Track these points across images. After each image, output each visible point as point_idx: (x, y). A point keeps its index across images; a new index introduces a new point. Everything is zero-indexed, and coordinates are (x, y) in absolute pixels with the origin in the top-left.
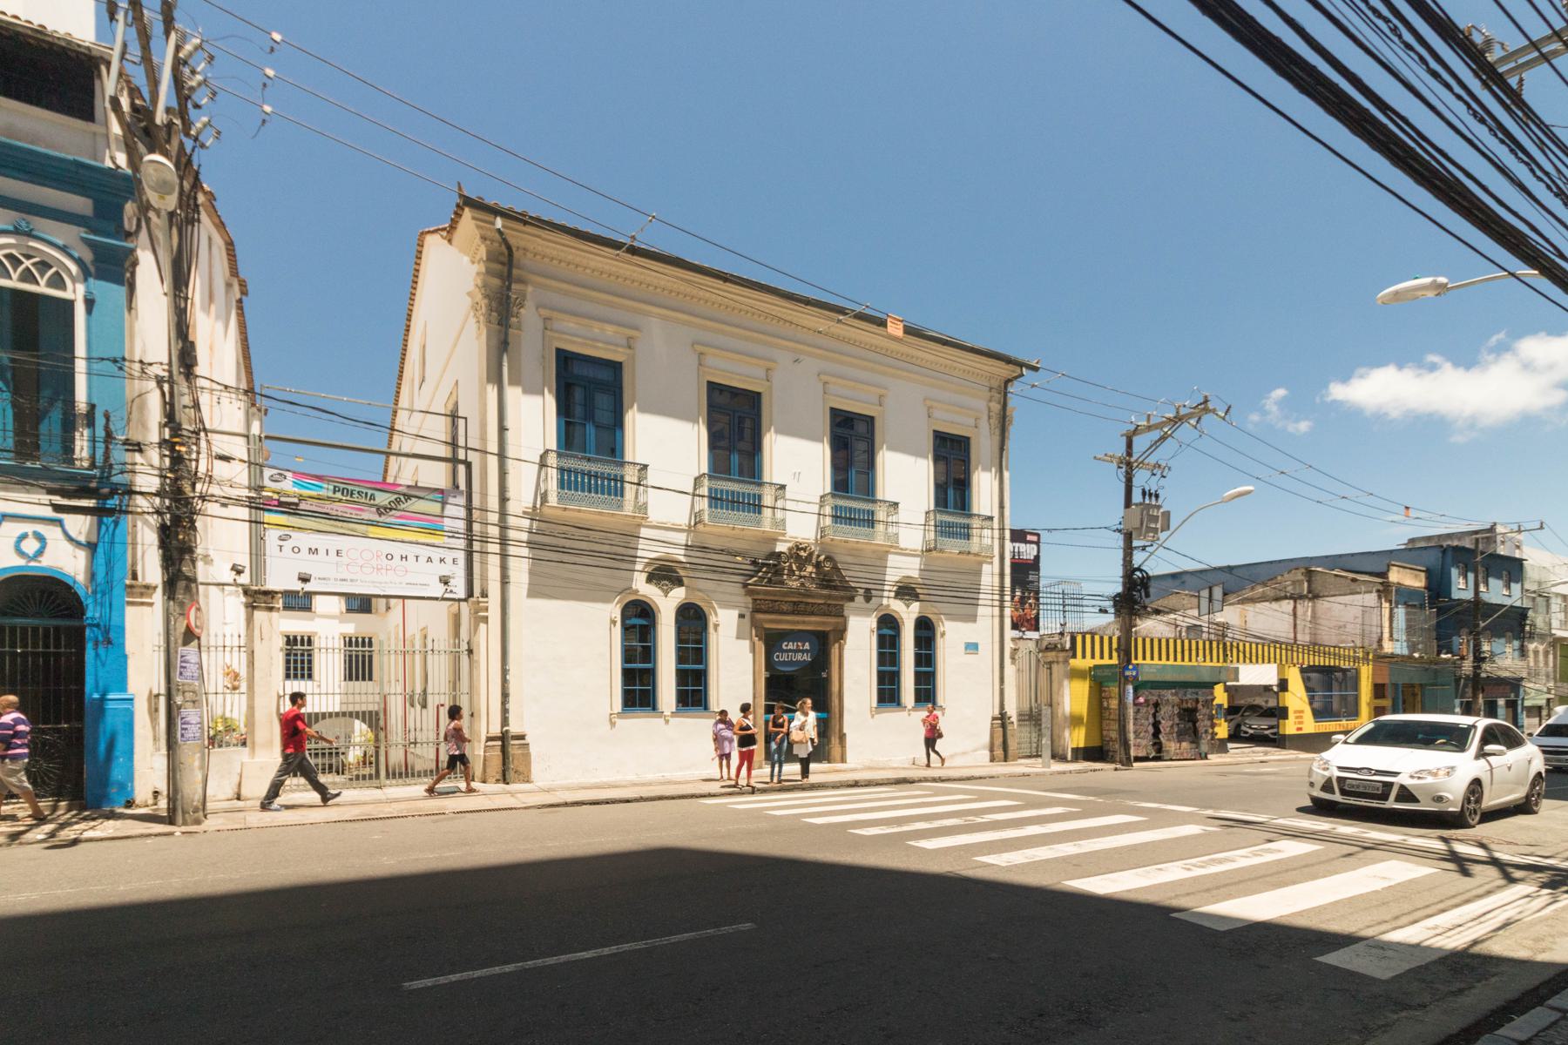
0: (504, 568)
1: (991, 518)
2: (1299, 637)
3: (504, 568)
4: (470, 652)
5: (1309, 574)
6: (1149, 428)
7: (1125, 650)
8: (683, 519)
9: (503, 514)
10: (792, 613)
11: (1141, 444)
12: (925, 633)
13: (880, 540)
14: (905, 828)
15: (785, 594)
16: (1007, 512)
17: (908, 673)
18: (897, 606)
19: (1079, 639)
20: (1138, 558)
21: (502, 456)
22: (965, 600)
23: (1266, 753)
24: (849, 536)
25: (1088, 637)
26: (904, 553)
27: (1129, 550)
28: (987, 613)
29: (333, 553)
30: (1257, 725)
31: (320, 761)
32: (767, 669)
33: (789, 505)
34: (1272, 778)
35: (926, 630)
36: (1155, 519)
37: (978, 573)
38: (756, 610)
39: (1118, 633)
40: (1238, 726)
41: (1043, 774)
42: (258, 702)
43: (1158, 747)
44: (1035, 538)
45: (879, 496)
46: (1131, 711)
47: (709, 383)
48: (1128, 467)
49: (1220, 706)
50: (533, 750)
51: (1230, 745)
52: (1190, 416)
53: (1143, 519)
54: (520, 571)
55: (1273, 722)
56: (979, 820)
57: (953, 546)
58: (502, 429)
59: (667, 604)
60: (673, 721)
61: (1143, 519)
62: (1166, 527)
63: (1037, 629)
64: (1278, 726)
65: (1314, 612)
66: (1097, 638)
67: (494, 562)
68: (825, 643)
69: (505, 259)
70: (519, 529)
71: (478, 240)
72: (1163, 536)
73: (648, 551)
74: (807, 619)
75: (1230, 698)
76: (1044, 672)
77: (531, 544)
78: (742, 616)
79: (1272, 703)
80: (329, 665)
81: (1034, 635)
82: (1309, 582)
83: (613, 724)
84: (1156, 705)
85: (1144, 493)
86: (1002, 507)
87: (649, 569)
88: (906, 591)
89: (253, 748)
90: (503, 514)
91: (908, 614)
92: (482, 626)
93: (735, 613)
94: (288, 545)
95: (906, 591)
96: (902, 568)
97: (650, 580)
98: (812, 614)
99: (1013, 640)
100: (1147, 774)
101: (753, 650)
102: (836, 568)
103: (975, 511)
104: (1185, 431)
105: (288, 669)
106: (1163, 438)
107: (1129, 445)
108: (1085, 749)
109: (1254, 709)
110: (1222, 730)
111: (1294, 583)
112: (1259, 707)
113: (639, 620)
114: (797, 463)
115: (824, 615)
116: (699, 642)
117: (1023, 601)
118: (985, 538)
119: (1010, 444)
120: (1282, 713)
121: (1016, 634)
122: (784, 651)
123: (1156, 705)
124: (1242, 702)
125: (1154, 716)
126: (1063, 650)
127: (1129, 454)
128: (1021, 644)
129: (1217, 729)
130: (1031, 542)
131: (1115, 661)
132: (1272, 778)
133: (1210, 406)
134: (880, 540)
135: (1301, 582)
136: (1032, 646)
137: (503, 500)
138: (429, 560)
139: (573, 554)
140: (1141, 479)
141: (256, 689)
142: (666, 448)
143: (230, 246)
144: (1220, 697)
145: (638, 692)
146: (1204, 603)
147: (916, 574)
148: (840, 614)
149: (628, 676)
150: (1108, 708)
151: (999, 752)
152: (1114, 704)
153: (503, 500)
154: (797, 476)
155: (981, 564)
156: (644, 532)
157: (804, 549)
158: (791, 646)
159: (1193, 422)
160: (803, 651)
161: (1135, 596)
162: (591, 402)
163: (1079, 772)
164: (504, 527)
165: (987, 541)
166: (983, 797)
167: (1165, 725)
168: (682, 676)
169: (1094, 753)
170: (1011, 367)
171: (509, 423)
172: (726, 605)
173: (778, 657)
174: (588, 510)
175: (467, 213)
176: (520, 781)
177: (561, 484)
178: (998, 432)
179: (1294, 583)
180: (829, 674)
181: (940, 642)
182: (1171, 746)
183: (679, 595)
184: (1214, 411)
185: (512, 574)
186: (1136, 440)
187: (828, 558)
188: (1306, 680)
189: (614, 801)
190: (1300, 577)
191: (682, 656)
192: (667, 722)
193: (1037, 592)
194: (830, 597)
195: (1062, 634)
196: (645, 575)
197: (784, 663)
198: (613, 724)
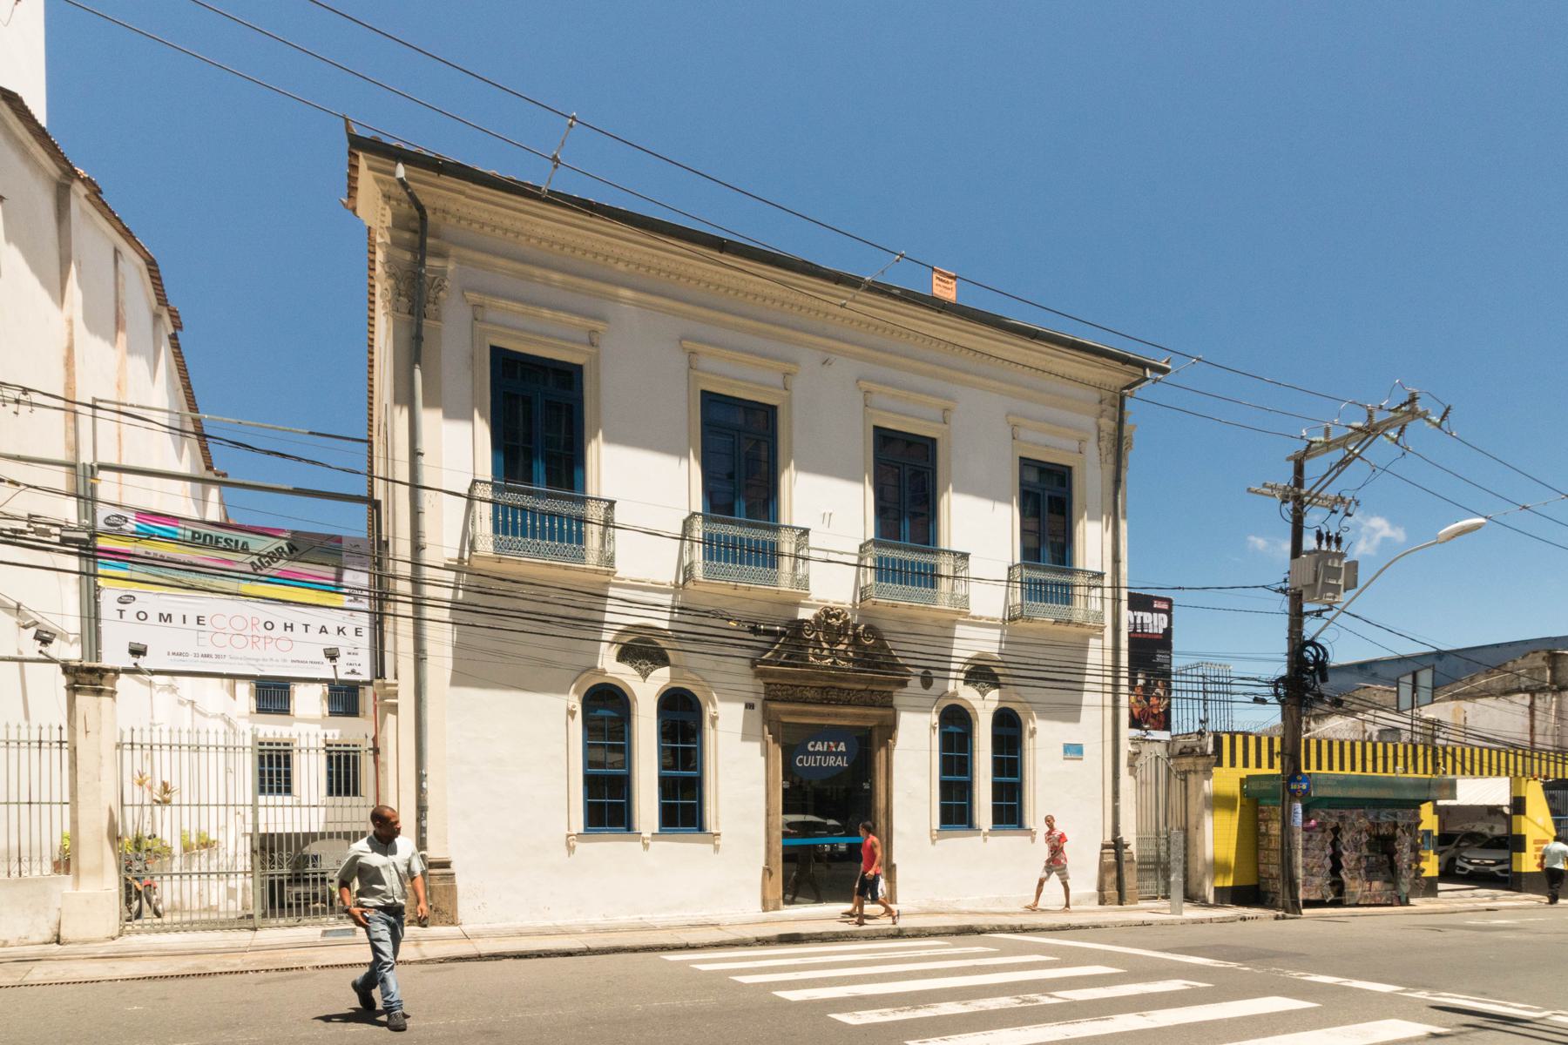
0: (418, 638)
1: (1101, 575)
2: (1538, 739)
3: (418, 638)
4: (376, 751)
5: (1553, 659)
6: (1328, 446)
7: (1292, 750)
8: (667, 574)
9: (416, 564)
10: (820, 703)
11: (1315, 468)
13: (944, 604)
14: (922, 1013)
15: (808, 677)
16: (1124, 568)
17: (987, 785)
18: (968, 694)
19: (1226, 739)
20: (1310, 628)
21: (415, 487)
22: (1062, 681)
23: (1494, 898)
24: (898, 601)
26: (977, 622)
27: (1297, 617)
28: (1095, 705)
29: (191, 621)
30: (1479, 859)
31: (302, 889)
33: (813, 554)
34: (1512, 936)
35: (1009, 731)
36: (1336, 573)
37: (1084, 648)
38: (770, 698)
39: (1280, 732)
40: (1452, 860)
41: (1172, 923)
42: (83, 815)
43: (1338, 886)
44: (1165, 606)
45: (943, 545)
46: (1299, 839)
47: (704, 393)
48: (1297, 501)
49: (1428, 833)
50: (461, 882)
51: (1441, 886)
52: (1389, 424)
53: (1319, 576)
54: (441, 639)
55: (1502, 854)
56: (1046, 1000)
57: (1046, 615)
58: (415, 454)
59: (645, 691)
61: (1319, 576)
62: (1352, 584)
63: (1167, 727)
64: (1510, 861)
65: (1559, 711)
66: (1252, 739)
67: (406, 627)
68: (869, 744)
69: (415, 225)
70: (437, 584)
71: (381, 203)
72: (1344, 597)
73: (618, 616)
75: (1442, 823)
76: (1176, 784)
77: (456, 606)
78: (749, 706)
79: (1500, 830)
80: (310, 772)
81: (1164, 736)
82: (1554, 670)
83: (571, 849)
84: (1336, 830)
85: (1319, 537)
86: (1116, 560)
87: (626, 639)
88: (980, 674)
89: (77, 876)
90: (416, 564)
91: (984, 706)
92: (391, 718)
94: (130, 609)
95: (980, 674)
96: (975, 642)
98: (848, 703)
99: (1134, 741)
100: (1321, 927)
101: (766, 753)
102: (880, 638)
103: (1079, 565)
104: (1381, 449)
105: (262, 781)
106: (1345, 462)
107: (1299, 470)
108: (1233, 888)
109: (1474, 838)
110: (1431, 866)
111: (1531, 671)
112: (1482, 835)
113: (606, 712)
114: (829, 509)
115: (866, 705)
117: (1147, 688)
118: (1093, 604)
119: (1127, 475)
120: (1516, 843)
121: (1136, 732)
122: (809, 753)
123: (1336, 830)
124: (1456, 829)
125: (1333, 844)
126: (1204, 754)
127: (1299, 482)
128: (1146, 748)
129: (1423, 865)
130: (1159, 611)
131: (1277, 770)
132: (1512, 936)
133: (1420, 407)
134: (944, 604)
135: (1541, 670)
136: (1160, 749)
137: (417, 548)
139: (510, 624)
140: (1314, 518)
141: (80, 799)
143: (152, 265)
144: (1429, 820)
145: (607, 806)
146: (1405, 691)
149: (593, 784)
150: (1267, 834)
151: (1111, 892)
152: (1275, 829)
153: (417, 548)
154: (827, 518)
155: (1087, 637)
157: (837, 617)
158: (819, 747)
159: (1393, 434)
160: (837, 754)
161: (1306, 683)
162: (540, 422)
163: (1223, 921)
164: (416, 581)
165: (1095, 605)
166: (1070, 957)
167: (1348, 858)
168: (667, 787)
169: (1246, 895)
171: (424, 446)
172: (727, 696)
173: (802, 762)
174: (534, 563)
175: (363, 161)
176: (441, 923)
178: (1111, 459)
179: (1531, 671)
180: (873, 785)
181: (1028, 743)
182: (1355, 886)
183: (661, 677)
184: (1425, 416)
185: (430, 647)
186: (1307, 464)
187: (870, 629)
188: (1551, 799)
189: (539, 955)
190: (1540, 662)
192: (646, 846)
193: (1168, 674)
195: (1200, 733)
196: (615, 650)
198: (571, 849)
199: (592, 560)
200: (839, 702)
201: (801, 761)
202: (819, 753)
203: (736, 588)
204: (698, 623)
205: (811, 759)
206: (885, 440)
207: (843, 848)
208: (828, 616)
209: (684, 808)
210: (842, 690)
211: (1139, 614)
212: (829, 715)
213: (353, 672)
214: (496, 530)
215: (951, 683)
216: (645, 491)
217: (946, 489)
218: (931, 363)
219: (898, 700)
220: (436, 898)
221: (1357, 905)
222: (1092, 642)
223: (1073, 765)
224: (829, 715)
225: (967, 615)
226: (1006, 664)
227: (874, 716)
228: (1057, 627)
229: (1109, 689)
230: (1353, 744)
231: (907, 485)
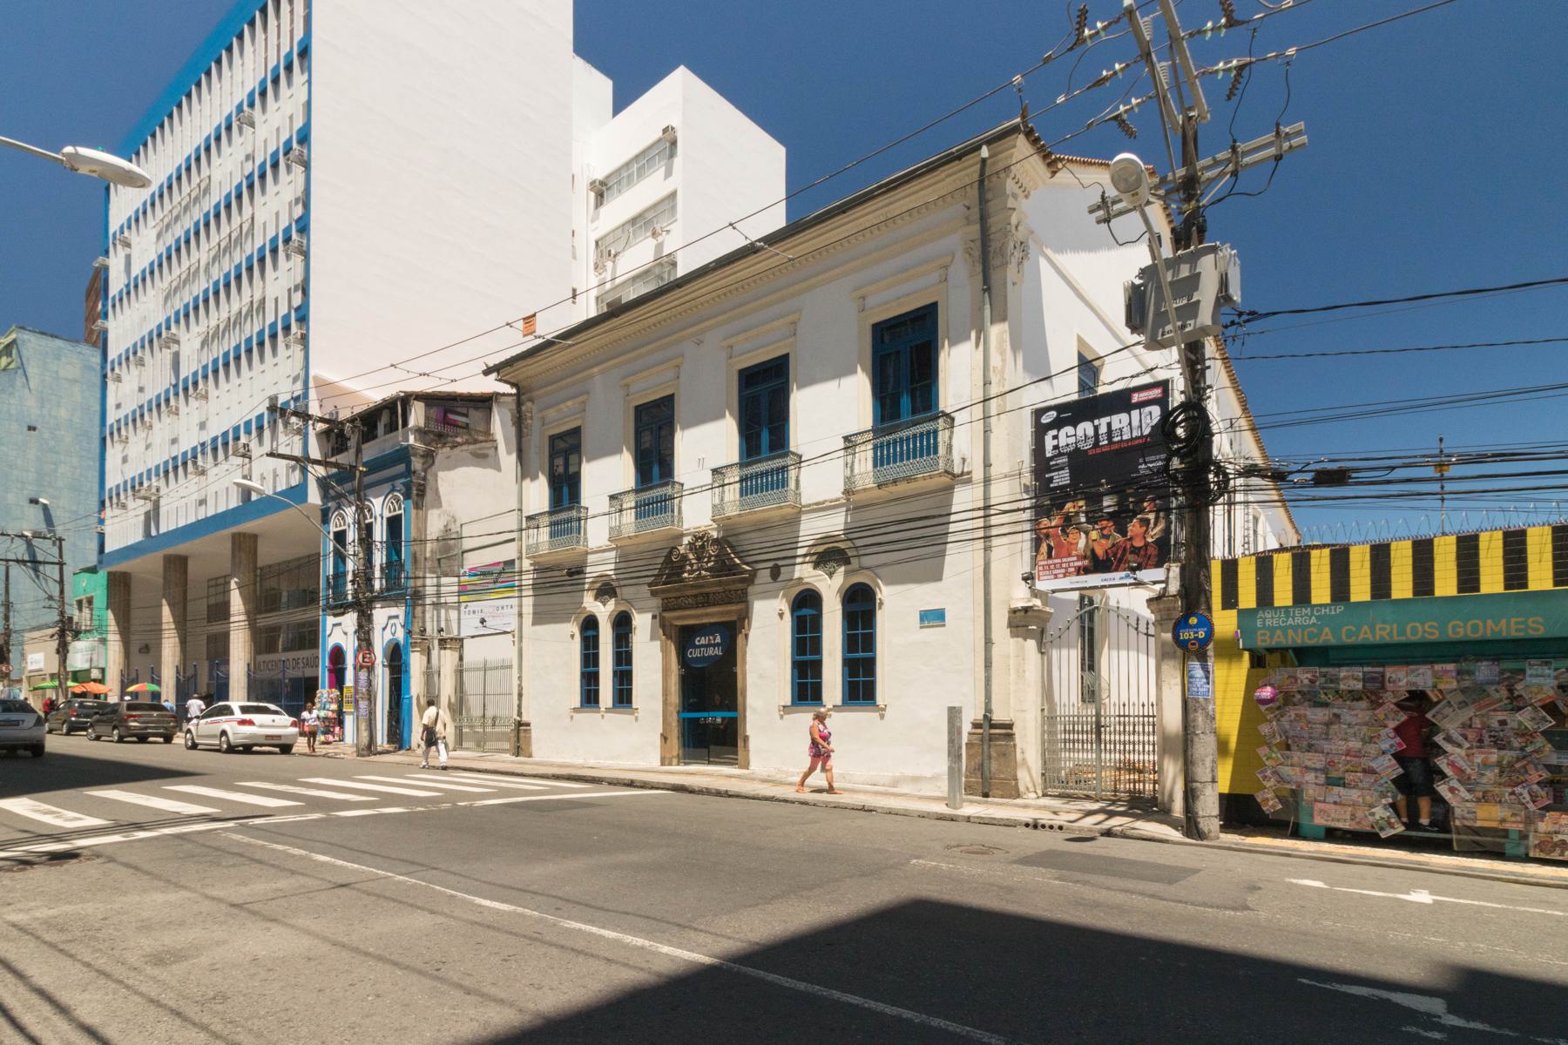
12: (590, 633)
24: (767, 507)
38: (666, 608)
60: (607, 715)
68: (732, 631)
74: (710, 610)
78: (654, 617)
88: (829, 555)
91: (830, 587)
93: (649, 616)
96: (813, 528)
101: (664, 650)
113: (590, 625)
142: (608, 476)
154: (701, 461)
160: (714, 645)
172: (641, 610)
173: (693, 654)
177: (552, 535)
178: (979, 268)
199: (791, 497)
211: (1104, 421)
214: (875, 466)
215: (798, 567)
221: (1527, 859)
223: (933, 634)
230: (1264, 563)
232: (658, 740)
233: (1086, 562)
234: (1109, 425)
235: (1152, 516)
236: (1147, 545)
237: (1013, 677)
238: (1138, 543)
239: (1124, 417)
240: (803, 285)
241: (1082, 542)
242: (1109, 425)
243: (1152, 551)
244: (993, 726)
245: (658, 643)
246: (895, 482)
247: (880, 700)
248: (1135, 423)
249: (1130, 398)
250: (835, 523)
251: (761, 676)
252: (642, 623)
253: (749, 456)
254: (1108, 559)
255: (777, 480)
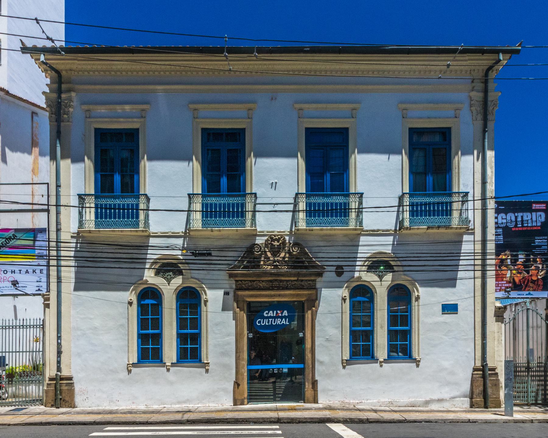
15: (258, 275)
18: (370, 278)
25: (46, 207)
32: (250, 330)
35: (401, 296)
38: (239, 288)
50: (77, 388)
54: (69, 274)
59: (168, 289)
60: (172, 369)
68: (302, 310)
74: (282, 292)
78: (226, 293)
83: (130, 372)
88: (377, 264)
91: (381, 286)
93: (221, 293)
96: (367, 247)
97: (157, 273)
98: (287, 288)
113: (149, 299)
116: (196, 314)
130: (537, 211)
138: (27, 272)
139: (102, 263)
145: (149, 351)
147: (388, 250)
148: (313, 287)
151: (479, 399)
156: (153, 241)
170: (486, 56)
176: (66, 407)
178: (480, 117)
183: (178, 281)
191: (181, 324)
192: (168, 370)
194: (298, 275)
197: (265, 327)
198: (130, 372)
200: (279, 288)
201: (260, 322)
202: (271, 317)
203: (212, 231)
204: (200, 254)
205: (266, 321)
206: (312, 134)
207: (285, 370)
208: (273, 240)
209: (191, 351)
210: (281, 281)
211: (520, 214)
212: (274, 296)
213: (39, 290)
214: (96, 217)
216: (170, 189)
217: (457, 154)
218: (343, 84)
219: (318, 285)
220: (64, 395)
222: (466, 238)
223: (449, 318)
224: (274, 296)
225: (362, 230)
226: (397, 258)
227: (305, 295)
228: (430, 231)
229: (479, 268)
231: (326, 161)
232: (230, 386)
233: (510, 285)
234: (522, 217)
235: (540, 266)
236: (538, 279)
237: (496, 343)
238: (534, 278)
239: (529, 214)
240: (353, 87)
241: (508, 275)
242: (522, 217)
243: (540, 283)
244: (62, 379)
245: (231, 313)
246: (439, 227)
247: (415, 355)
248: (534, 219)
249: (531, 206)
250: (385, 245)
251: (327, 340)
252: (213, 298)
253: (103, 191)
254: (521, 284)
255: (131, 214)
